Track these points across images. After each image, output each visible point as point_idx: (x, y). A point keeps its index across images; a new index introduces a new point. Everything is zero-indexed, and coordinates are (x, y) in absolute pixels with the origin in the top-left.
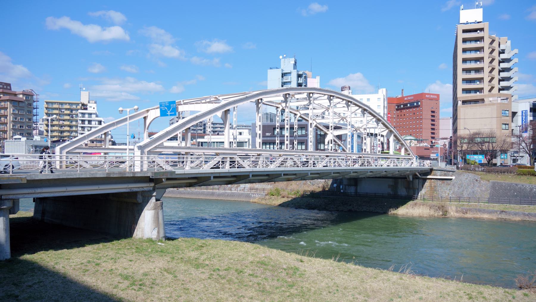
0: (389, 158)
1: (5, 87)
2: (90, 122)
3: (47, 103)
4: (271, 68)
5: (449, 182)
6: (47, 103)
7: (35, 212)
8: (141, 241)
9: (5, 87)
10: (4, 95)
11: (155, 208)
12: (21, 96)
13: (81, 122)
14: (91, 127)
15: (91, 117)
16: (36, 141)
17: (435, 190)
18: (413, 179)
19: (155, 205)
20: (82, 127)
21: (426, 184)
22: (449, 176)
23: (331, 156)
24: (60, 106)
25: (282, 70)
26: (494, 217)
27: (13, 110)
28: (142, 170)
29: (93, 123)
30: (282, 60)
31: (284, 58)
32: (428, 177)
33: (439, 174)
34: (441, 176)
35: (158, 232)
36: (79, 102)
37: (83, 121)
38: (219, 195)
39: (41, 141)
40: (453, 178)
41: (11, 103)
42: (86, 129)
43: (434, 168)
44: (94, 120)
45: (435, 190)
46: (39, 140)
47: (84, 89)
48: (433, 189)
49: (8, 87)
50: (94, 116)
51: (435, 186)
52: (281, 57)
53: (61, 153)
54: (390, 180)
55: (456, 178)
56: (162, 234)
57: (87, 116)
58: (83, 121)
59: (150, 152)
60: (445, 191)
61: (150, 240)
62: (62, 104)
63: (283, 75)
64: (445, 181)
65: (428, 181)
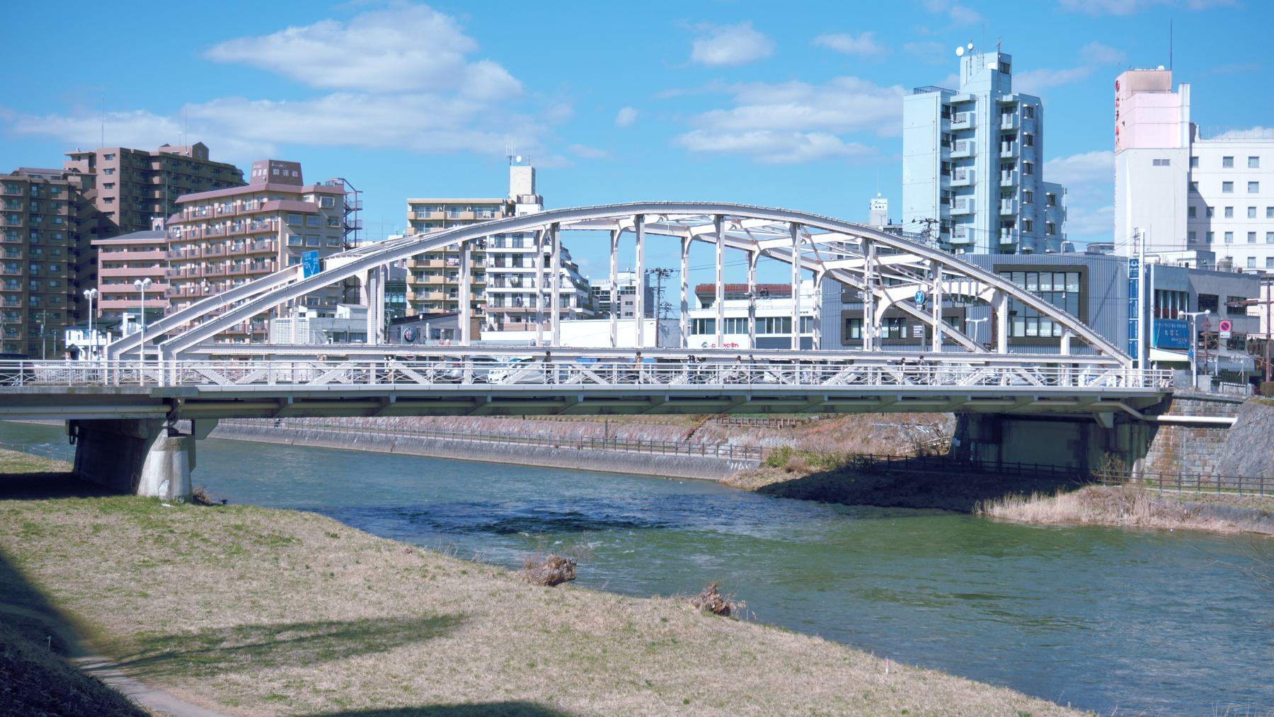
0: (810, 362)
1: (286, 173)
2: (518, 259)
3: (415, 207)
4: (917, 91)
5: (1221, 432)
6: (415, 207)
7: (79, 462)
8: (144, 499)
9: (286, 173)
10: (270, 199)
11: (167, 448)
12: (311, 199)
13: (492, 260)
14: (521, 275)
15: (520, 245)
16: (341, 319)
17: (1176, 457)
18: (1116, 423)
19: (167, 443)
20: (497, 276)
21: (1157, 437)
22: (1221, 414)
23: (859, 361)
24: (449, 214)
25: (945, 93)
26: (1244, 527)
27: (291, 238)
28: (167, 384)
29: (527, 261)
30: (964, 60)
31: (969, 53)
32: (1160, 418)
33: (1186, 409)
34: (1193, 414)
35: (170, 487)
36: (499, 200)
37: (499, 258)
38: (660, 464)
39: (351, 319)
40: (1233, 420)
41: (284, 219)
42: (507, 282)
43: (1177, 392)
44: (529, 254)
45: (1176, 457)
46: (348, 317)
47: (519, 159)
48: (1171, 454)
49: (295, 174)
50: (528, 243)
51: (1176, 445)
52: (960, 51)
53: (110, 357)
54: (1073, 425)
55: (1239, 421)
56: (177, 490)
57: (509, 241)
58: (499, 258)
59: (181, 356)
60: (1208, 460)
61: (156, 500)
62: (454, 207)
63: (948, 111)
64: (1208, 431)
65: (1162, 429)
